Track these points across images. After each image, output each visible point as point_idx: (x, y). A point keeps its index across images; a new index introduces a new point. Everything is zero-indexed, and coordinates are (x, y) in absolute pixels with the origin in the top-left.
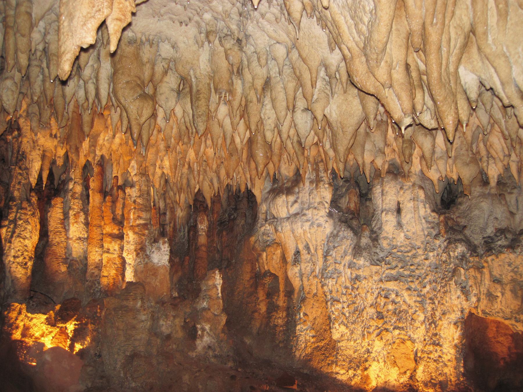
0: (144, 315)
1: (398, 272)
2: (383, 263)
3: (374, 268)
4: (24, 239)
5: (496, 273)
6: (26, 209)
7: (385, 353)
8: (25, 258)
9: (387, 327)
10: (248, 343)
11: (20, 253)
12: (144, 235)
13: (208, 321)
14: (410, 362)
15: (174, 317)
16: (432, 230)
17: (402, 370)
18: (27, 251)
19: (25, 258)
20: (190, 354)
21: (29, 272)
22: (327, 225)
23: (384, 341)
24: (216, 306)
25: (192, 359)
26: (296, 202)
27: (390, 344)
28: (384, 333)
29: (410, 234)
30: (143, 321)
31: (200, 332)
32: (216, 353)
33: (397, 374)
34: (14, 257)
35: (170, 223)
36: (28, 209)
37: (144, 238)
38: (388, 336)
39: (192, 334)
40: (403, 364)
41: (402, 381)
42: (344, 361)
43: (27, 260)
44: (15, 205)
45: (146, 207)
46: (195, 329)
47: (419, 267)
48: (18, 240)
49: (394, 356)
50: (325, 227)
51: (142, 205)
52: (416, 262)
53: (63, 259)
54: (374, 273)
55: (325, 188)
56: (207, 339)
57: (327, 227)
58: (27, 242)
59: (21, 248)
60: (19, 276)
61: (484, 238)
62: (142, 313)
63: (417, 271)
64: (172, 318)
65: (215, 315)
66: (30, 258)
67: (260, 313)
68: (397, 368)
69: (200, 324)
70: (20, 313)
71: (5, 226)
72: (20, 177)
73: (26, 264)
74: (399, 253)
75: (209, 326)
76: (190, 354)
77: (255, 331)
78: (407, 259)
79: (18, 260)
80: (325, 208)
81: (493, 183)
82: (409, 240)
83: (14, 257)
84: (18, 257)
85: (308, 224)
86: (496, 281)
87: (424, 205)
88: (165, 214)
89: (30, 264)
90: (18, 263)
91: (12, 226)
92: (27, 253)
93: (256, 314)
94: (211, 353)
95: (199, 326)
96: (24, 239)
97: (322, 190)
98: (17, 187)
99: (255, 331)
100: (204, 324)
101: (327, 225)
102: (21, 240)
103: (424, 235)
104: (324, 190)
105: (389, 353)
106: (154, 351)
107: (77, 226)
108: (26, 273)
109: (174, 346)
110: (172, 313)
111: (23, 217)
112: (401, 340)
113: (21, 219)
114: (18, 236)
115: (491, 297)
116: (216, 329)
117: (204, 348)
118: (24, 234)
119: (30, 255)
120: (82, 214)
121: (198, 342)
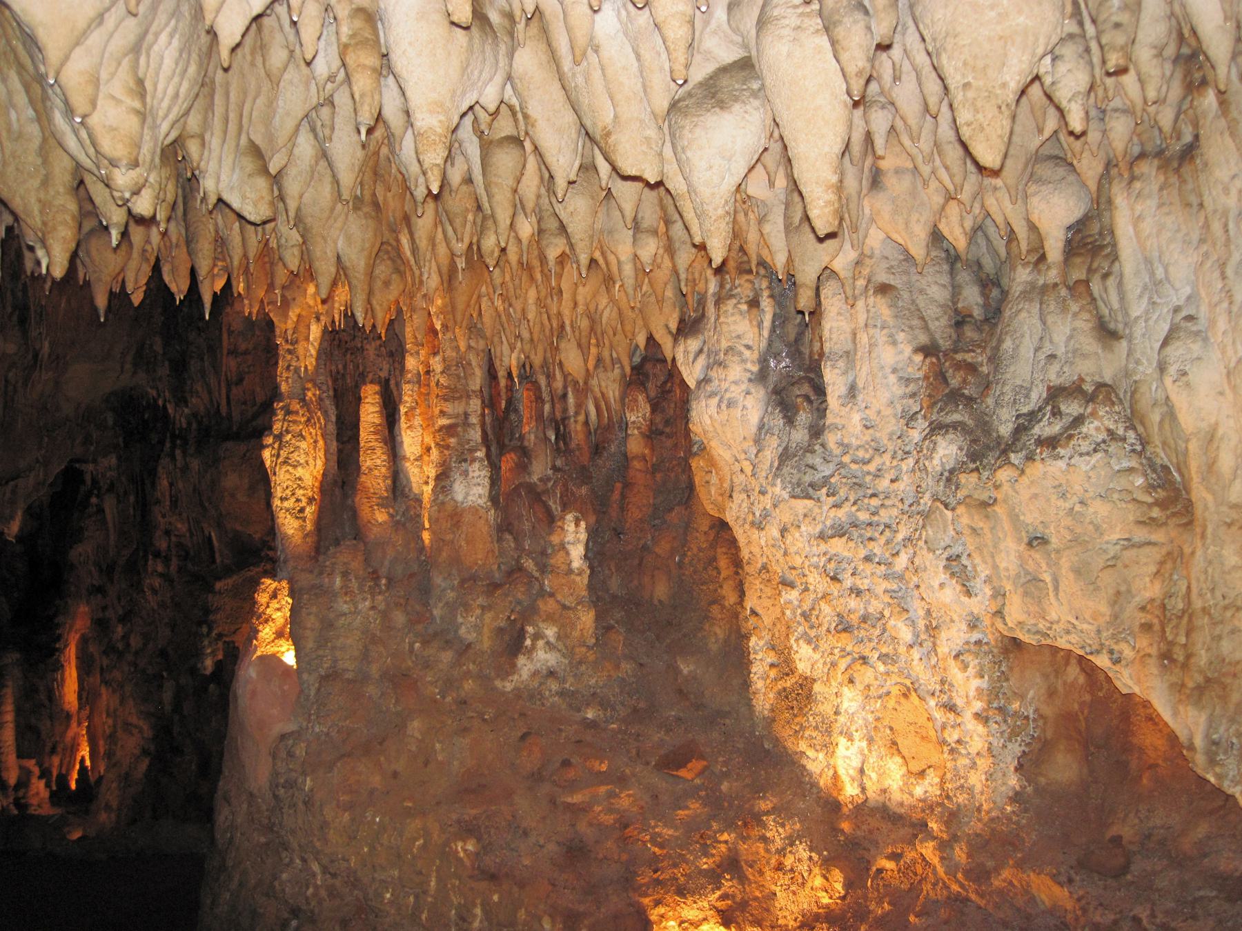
0: (345, 602)
1: (850, 515)
2: (824, 490)
3: (802, 505)
4: (295, 467)
5: (1031, 517)
6: (297, 413)
7: (870, 718)
8: (298, 500)
9: (867, 653)
10: (685, 671)
11: (288, 492)
12: (448, 447)
13: (550, 618)
14: (930, 746)
15: (483, 608)
16: (911, 401)
17: (915, 767)
18: (300, 487)
19: (298, 500)
20: (498, 683)
21: (309, 526)
22: (750, 402)
23: (860, 686)
24: (566, 589)
25: (503, 693)
26: (701, 351)
27: (880, 697)
28: (857, 666)
29: (871, 413)
30: (345, 614)
31: (528, 642)
32: (567, 686)
33: (901, 773)
34: (282, 499)
35: (577, 413)
36: (301, 412)
37: (446, 452)
38: (866, 675)
39: (513, 643)
40: (914, 750)
41: (919, 791)
42: (816, 728)
43: (303, 504)
44: (282, 408)
45: (454, 390)
46: (521, 634)
47: (887, 502)
48: (285, 468)
49: (891, 729)
50: (744, 407)
51: (446, 388)
52: (880, 489)
53: (380, 498)
54: (801, 518)
55: (741, 313)
56: (544, 657)
57: (749, 406)
58: (300, 472)
59: (290, 483)
60: (290, 532)
61: (1018, 417)
62: (340, 600)
63: (882, 512)
64: (478, 612)
65: (564, 607)
66: (311, 500)
67: (723, 607)
68: (898, 760)
69: (534, 625)
70: (274, 596)
71: (267, 446)
72: (289, 357)
73: (302, 510)
74: (853, 466)
75: (555, 629)
76: (498, 683)
77: (714, 647)
78: (868, 479)
79: (286, 504)
80: (744, 361)
81: (1054, 249)
82: (871, 431)
83: (282, 499)
84: (287, 499)
85: (715, 401)
86: (1035, 543)
87: (891, 336)
88: (565, 396)
89: (310, 511)
90: (287, 510)
91: (276, 446)
92: (301, 492)
93: (715, 609)
94: (554, 686)
95: (530, 629)
96: (295, 467)
97: (731, 319)
98: (285, 375)
99: (714, 647)
100: (541, 625)
101: (750, 402)
102: (290, 468)
103: (895, 415)
104: (737, 317)
105: (878, 719)
106: (374, 670)
107: (412, 434)
108: (302, 528)
109: (471, 666)
110: (481, 600)
111: (293, 428)
112: (904, 690)
113: (288, 432)
114: (285, 462)
115: (1031, 584)
116: (567, 636)
117: (535, 674)
118: (295, 456)
119: (310, 494)
120: (692, 383)
121: (521, 660)
